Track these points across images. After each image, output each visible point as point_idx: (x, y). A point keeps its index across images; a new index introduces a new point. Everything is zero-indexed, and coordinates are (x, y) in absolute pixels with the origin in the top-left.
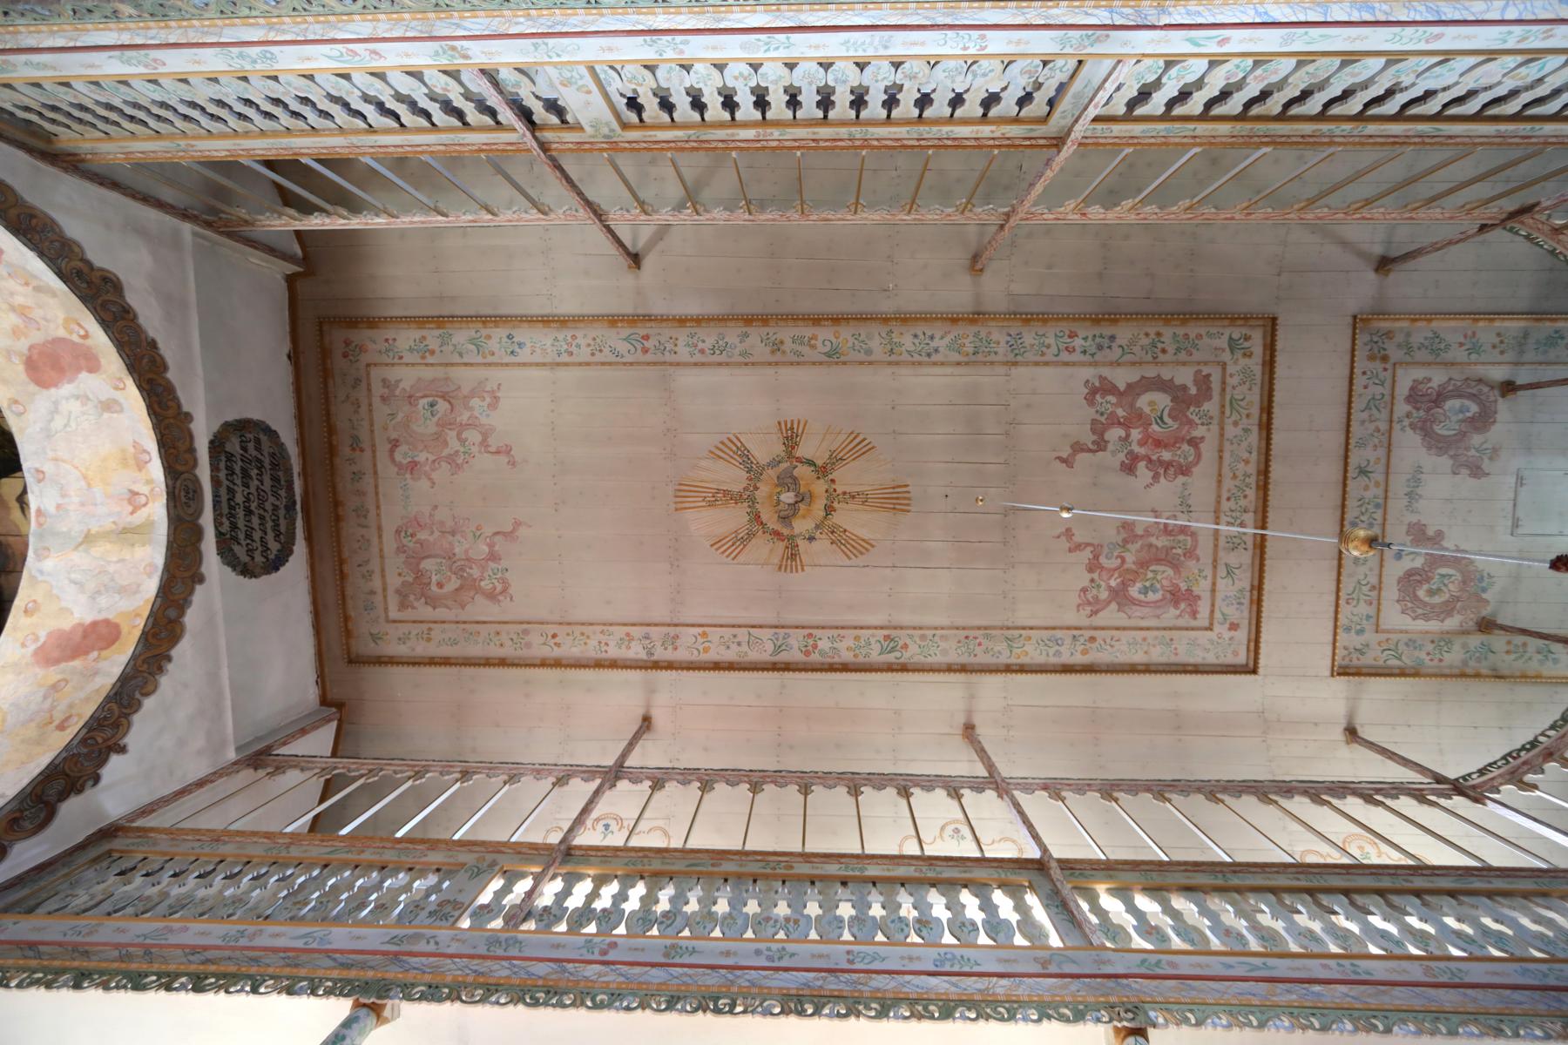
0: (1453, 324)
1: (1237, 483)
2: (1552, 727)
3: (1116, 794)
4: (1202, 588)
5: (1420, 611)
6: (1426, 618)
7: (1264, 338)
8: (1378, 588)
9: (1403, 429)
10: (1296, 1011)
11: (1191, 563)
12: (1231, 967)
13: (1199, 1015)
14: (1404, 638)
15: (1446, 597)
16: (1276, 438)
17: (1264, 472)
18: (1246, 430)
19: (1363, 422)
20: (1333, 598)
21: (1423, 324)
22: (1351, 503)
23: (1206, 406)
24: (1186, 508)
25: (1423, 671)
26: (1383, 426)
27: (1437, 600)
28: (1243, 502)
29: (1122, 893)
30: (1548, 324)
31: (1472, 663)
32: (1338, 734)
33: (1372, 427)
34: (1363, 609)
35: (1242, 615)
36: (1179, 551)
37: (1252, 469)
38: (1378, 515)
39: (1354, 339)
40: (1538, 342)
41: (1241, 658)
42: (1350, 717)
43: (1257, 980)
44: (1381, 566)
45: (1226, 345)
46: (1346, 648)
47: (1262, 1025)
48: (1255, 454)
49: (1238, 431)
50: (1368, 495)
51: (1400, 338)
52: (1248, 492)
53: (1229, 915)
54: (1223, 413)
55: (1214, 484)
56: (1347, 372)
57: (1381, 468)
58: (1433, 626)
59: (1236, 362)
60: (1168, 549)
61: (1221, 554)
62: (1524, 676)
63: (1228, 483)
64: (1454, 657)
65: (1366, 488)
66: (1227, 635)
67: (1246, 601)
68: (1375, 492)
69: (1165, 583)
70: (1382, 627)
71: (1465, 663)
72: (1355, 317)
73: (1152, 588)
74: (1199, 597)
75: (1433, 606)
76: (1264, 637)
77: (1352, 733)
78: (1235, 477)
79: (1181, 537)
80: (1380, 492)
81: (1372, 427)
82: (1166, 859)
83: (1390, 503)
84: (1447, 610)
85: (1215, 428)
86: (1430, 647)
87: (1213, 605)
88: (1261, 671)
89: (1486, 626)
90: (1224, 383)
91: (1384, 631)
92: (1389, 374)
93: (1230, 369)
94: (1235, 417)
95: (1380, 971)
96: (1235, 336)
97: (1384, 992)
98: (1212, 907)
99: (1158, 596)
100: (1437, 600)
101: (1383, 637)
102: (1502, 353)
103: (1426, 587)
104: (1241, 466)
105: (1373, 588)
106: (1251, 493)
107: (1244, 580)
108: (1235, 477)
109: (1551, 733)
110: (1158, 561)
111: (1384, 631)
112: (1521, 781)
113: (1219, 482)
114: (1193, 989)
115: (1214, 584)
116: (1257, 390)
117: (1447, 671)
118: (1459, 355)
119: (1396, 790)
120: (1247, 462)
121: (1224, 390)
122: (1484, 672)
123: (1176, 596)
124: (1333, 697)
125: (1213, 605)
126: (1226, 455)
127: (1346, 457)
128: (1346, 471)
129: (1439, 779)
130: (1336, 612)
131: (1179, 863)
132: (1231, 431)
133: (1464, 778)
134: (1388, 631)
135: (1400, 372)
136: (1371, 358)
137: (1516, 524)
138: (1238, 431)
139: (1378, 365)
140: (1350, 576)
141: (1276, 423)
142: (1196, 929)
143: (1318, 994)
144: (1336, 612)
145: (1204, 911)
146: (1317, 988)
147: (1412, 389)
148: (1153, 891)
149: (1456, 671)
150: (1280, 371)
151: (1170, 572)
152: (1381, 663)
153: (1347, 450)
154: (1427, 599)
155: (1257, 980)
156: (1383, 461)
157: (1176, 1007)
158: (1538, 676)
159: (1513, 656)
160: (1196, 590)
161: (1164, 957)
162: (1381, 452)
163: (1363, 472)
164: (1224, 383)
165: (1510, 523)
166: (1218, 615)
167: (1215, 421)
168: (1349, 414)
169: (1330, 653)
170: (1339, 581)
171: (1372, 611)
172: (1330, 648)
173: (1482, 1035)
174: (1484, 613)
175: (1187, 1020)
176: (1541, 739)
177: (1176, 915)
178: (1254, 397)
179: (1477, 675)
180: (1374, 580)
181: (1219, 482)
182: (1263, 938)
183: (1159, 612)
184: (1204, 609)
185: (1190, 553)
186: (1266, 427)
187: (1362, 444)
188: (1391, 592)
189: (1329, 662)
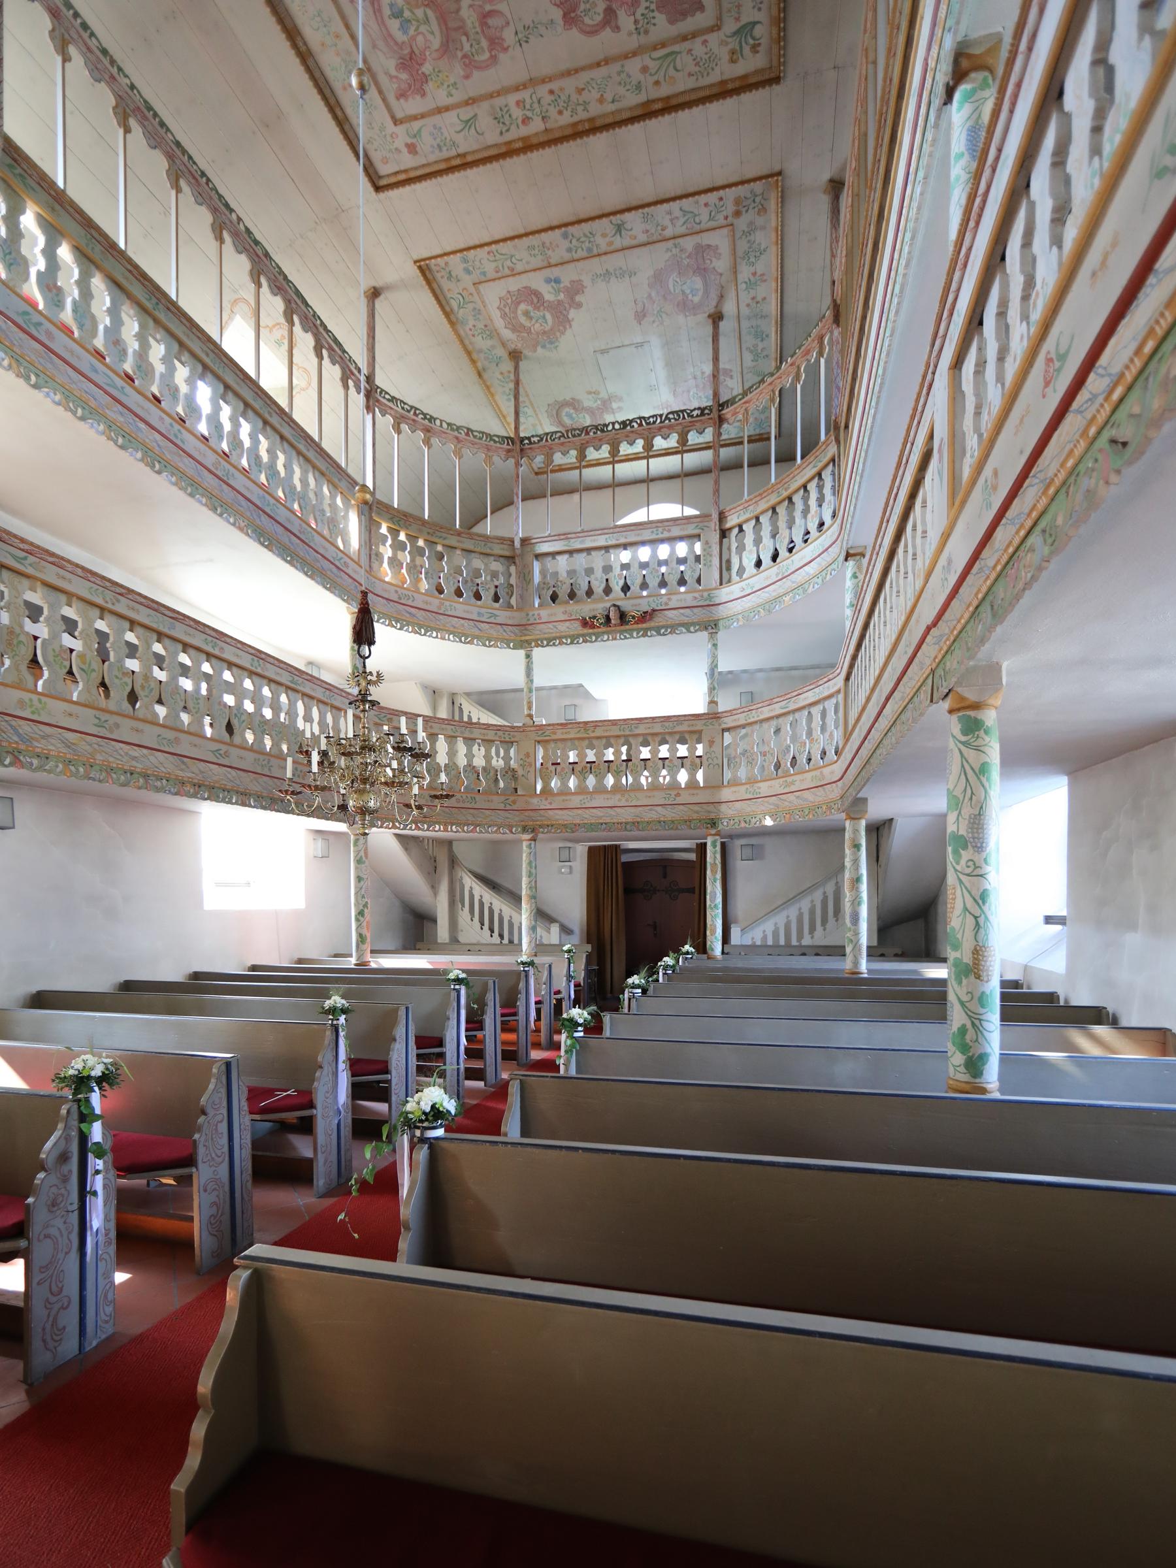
0: (774, 262)
1: (574, 97)
2: (449, 424)
3: (132, 122)
4: (438, 95)
5: (507, 310)
6: (504, 316)
7: (757, 72)
8: (514, 274)
9: (668, 250)
10: (114, 427)
11: (459, 70)
12: (96, 371)
13: (41, 381)
14: (479, 305)
15: (527, 324)
16: (636, 128)
17: (594, 128)
18: (639, 87)
19: (670, 213)
20: (487, 240)
21: (774, 239)
22: (585, 227)
23: (661, 19)
24: (526, 35)
25: (459, 327)
26: (669, 233)
27: (523, 319)
28: (553, 112)
29: (54, 234)
30: (773, 329)
31: (482, 356)
32: (365, 283)
33: (667, 222)
34: (490, 268)
35: (429, 154)
36: (467, 47)
37: (595, 110)
38: (581, 253)
39: (755, 180)
40: (757, 326)
41: (384, 169)
42: (388, 288)
43: (106, 392)
44: (535, 270)
45: (744, 20)
46: (446, 264)
47: (82, 419)
48: (612, 107)
49: (637, 76)
50: (599, 240)
51: (760, 221)
52: (567, 114)
53: (131, 327)
54: (655, 48)
55: (564, 67)
56: (720, 183)
57: (627, 242)
58: (499, 323)
59: (723, 43)
60: (462, 29)
61: (485, 105)
62: (488, 388)
63: (570, 84)
64: (481, 343)
65: (604, 235)
66: (400, 143)
67: (445, 154)
68: (603, 244)
69: (420, 39)
70: (481, 287)
71: (480, 351)
72: (779, 173)
73: (405, 25)
74: (424, 95)
75: (516, 317)
76: (418, 187)
77: (375, 294)
78: (580, 91)
79: (484, 43)
80: (604, 248)
81: (667, 222)
82: (122, 245)
83: (596, 260)
84: (516, 328)
85: (633, 42)
86: (480, 325)
87: (423, 116)
88: (382, 195)
89: (515, 356)
90: (694, 35)
91: (478, 290)
92: (722, 222)
93: (713, 38)
94: (654, 65)
95: (191, 444)
96: (758, 31)
97: (180, 456)
98: (124, 316)
99: (400, 37)
100: (523, 319)
101: (472, 289)
102: (748, 305)
103: (530, 308)
104: (595, 95)
105: (513, 270)
106: (566, 119)
107: (467, 144)
108: (580, 91)
109: (445, 426)
110: (443, 19)
111: (478, 290)
112: (399, 424)
113: (568, 73)
114: (52, 362)
115: (447, 109)
116: (691, 83)
117: (467, 342)
118: (745, 272)
119: (339, 355)
120: (601, 100)
121: (685, 38)
122: (479, 364)
123: (410, 61)
124: (396, 267)
125: (423, 116)
126: (603, 71)
127: (629, 210)
128: (614, 213)
129: (370, 379)
130: (475, 247)
131: (130, 261)
132: (634, 66)
133: (382, 390)
134: (479, 293)
135: (725, 231)
136: (738, 201)
137: (603, 352)
138: (637, 76)
139: (730, 208)
140: (515, 247)
141: (652, 123)
142: (93, 318)
143: (139, 429)
144: (475, 247)
145: (114, 312)
146: (142, 425)
147: (709, 246)
148: (81, 254)
149: (470, 348)
150: (714, 107)
151: (436, 43)
152: (449, 296)
153: (636, 208)
154: (519, 312)
155: (106, 392)
156: (634, 242)
157: (25, 364)
158: (492, 395)
159: (500, 377)
160: (430, 87)
161: (47, 325)
162: (642, 238)
163: (619, 228)
164: (694, 35)
165: (603, 347)
166: (416, 125)
167: (643, 39)
168: (674, 199)
169: (434, 253)
170: (505, 240)
171: (491, 274)
172: (439, 252)
173: (206, 505)
174: (526, 352)
175: (27, 379)
176: (438, 422)
177: (86, 294)
178: (682, 84)
179: (473, 362)
180: (519, 267)
181: (568, 73)
182: (139, 367)
183: (380, 44)
184: (413, 105)
185: (470, 64)
186: (648, 112)
187: (645, 218)
188: (514, 284)
189: (428, 255)
